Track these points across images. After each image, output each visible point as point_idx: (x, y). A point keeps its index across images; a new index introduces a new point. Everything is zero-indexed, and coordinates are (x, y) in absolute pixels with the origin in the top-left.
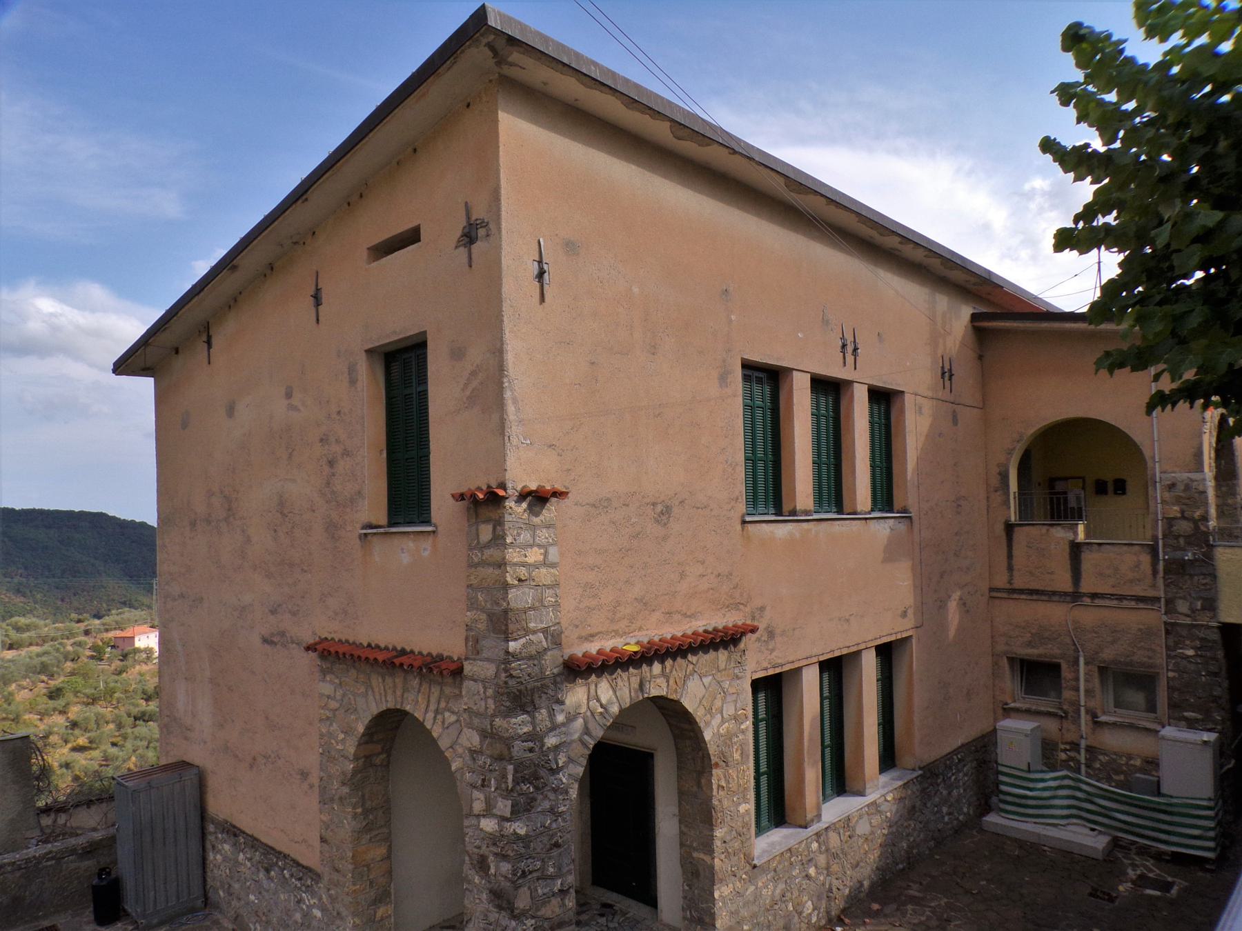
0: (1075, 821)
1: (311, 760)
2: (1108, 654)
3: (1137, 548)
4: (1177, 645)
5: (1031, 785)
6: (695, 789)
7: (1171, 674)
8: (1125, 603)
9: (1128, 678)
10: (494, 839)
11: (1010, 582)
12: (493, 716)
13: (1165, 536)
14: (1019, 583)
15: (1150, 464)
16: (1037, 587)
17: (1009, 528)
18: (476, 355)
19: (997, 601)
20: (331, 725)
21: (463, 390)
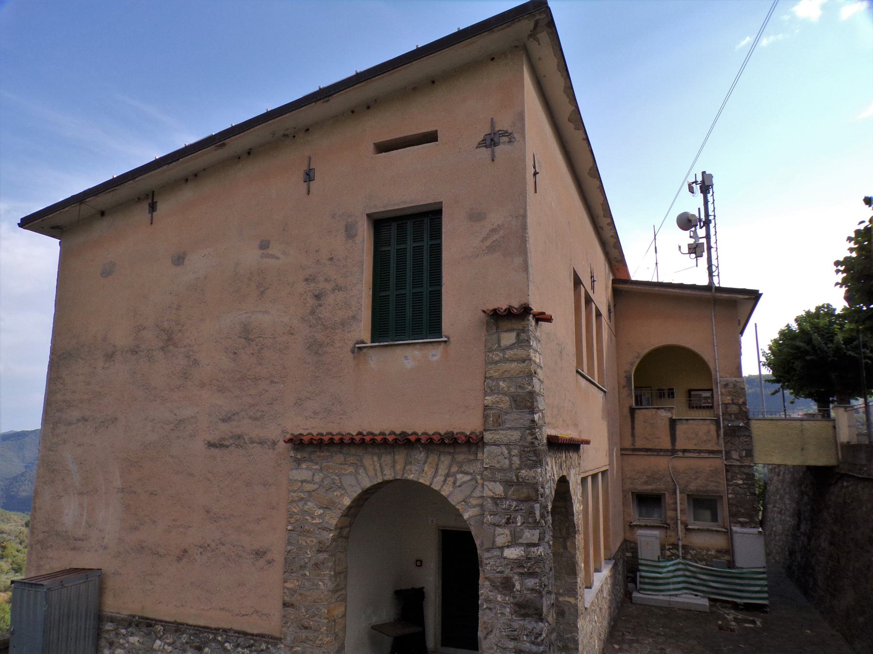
0: (685, 591)
1: (275, 540)
2: (693, 486)
3: (708, 422)
4: (733, 478)
5: (660, 570)
6: (561, 550)
7: (730, 496)
8: (703, 455)
9: (703, 503)
10: (518, 563)
11: (633, 444)
12: (520, 468)
13: (723, 414)
14: (638, 445)
15: (713, 373)
16: (650, 447)
17: (632, 411)
18: (497, 217)
19: (625, 457)
20: (305, 504)
21: (482, 241)
